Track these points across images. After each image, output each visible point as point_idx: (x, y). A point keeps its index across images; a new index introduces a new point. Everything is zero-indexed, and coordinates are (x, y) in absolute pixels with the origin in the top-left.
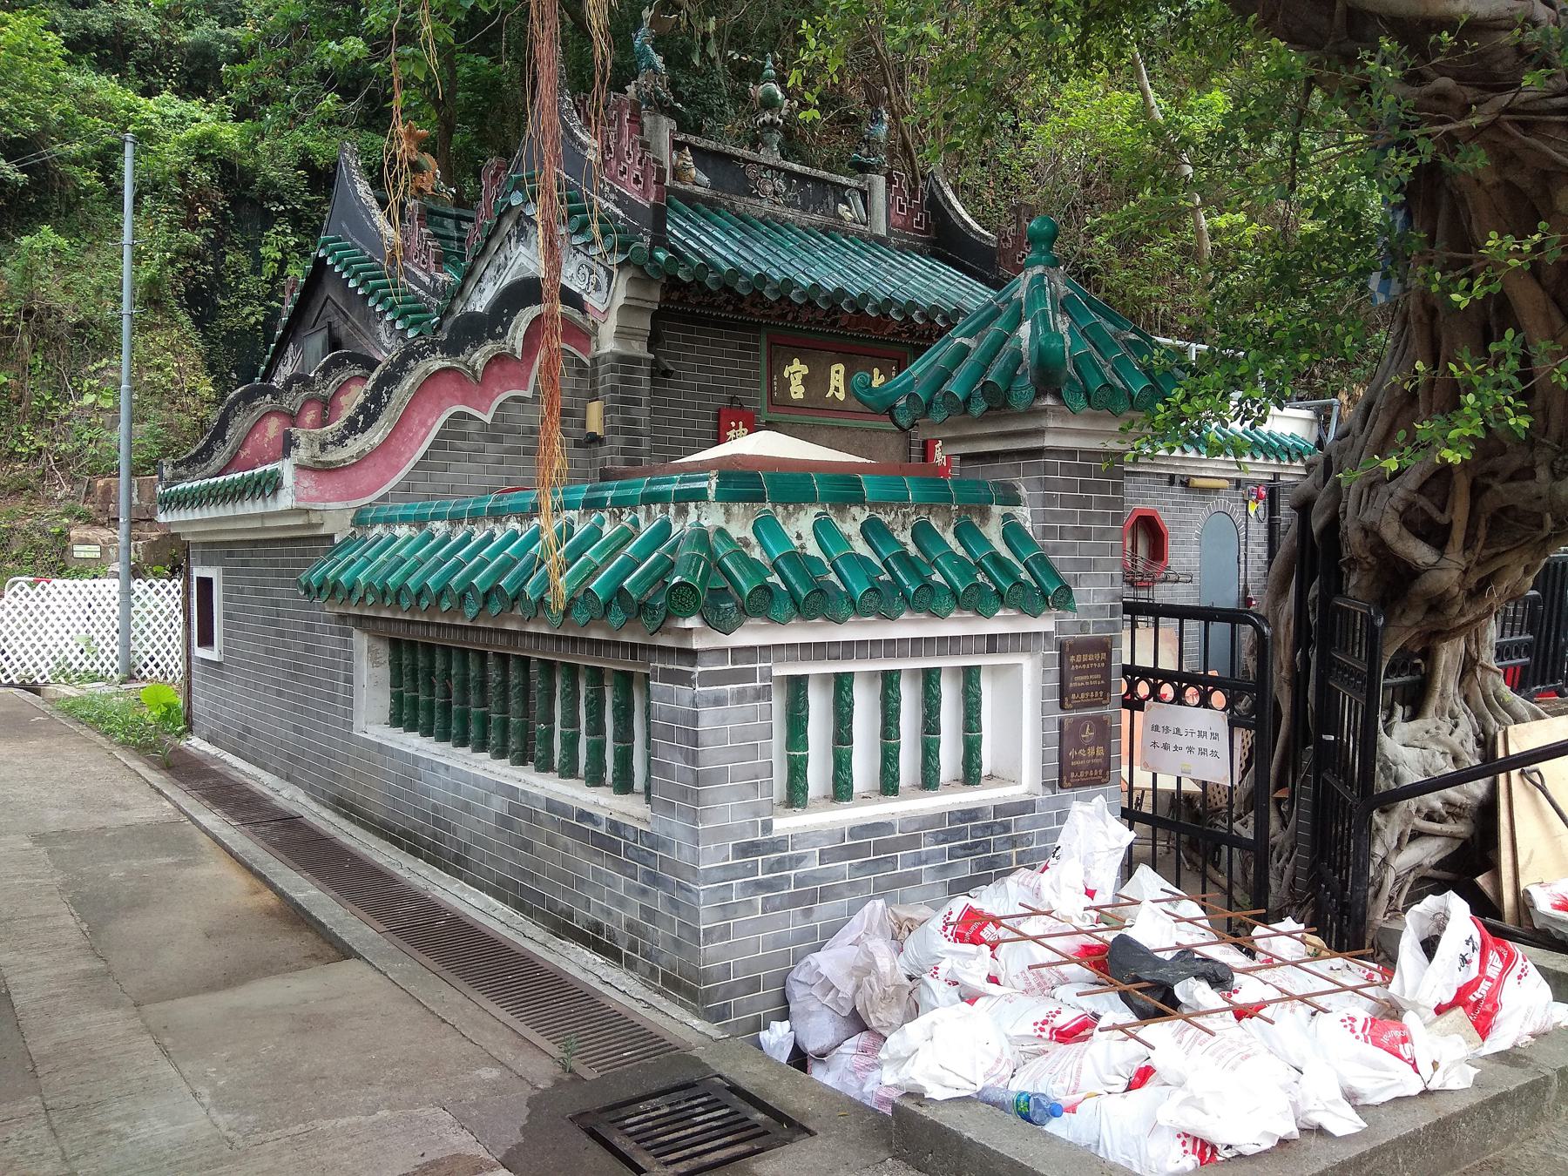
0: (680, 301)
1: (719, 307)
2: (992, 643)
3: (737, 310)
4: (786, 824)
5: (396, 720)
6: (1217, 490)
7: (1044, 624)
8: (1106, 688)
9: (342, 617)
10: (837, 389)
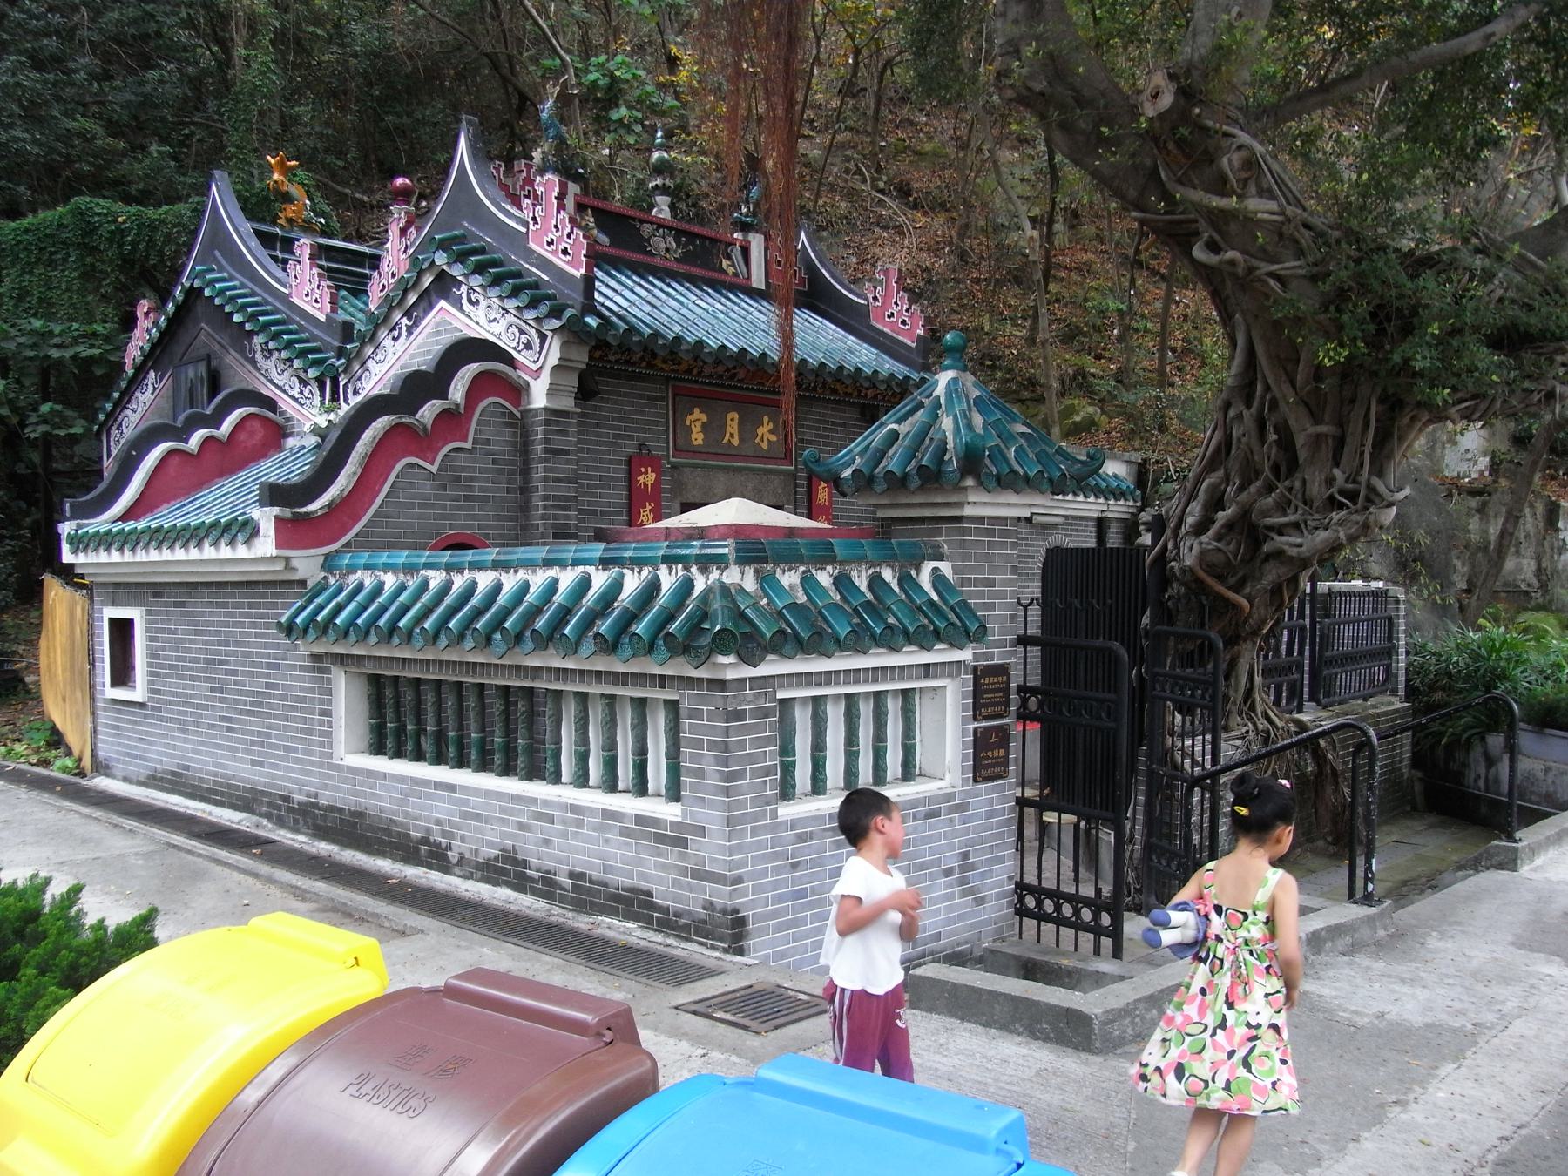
0: (601, 358)
1: (634, 364)
2: (928, 670)
3: (650, 366)
4: (786, 811)
5: (378, 749)
6: (1055, 526)
7: (966, 655)
8: (1007, 704)
9: (316, 657)
10: (732, 435)
